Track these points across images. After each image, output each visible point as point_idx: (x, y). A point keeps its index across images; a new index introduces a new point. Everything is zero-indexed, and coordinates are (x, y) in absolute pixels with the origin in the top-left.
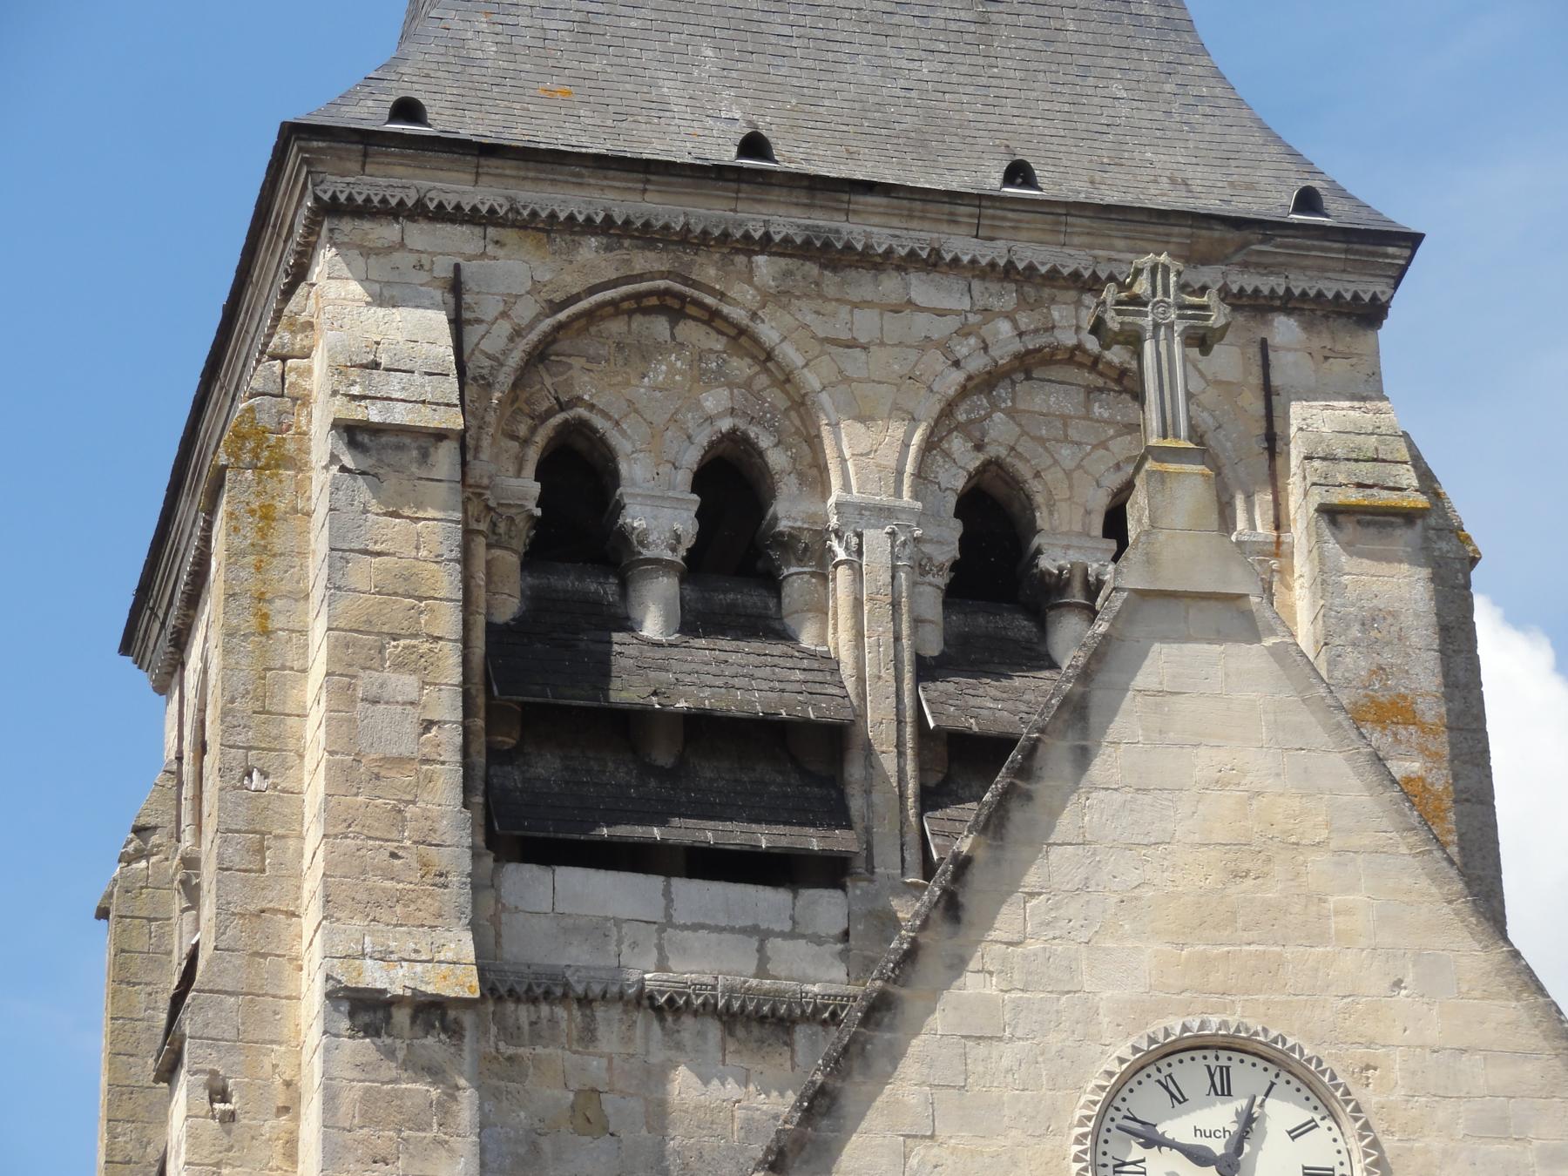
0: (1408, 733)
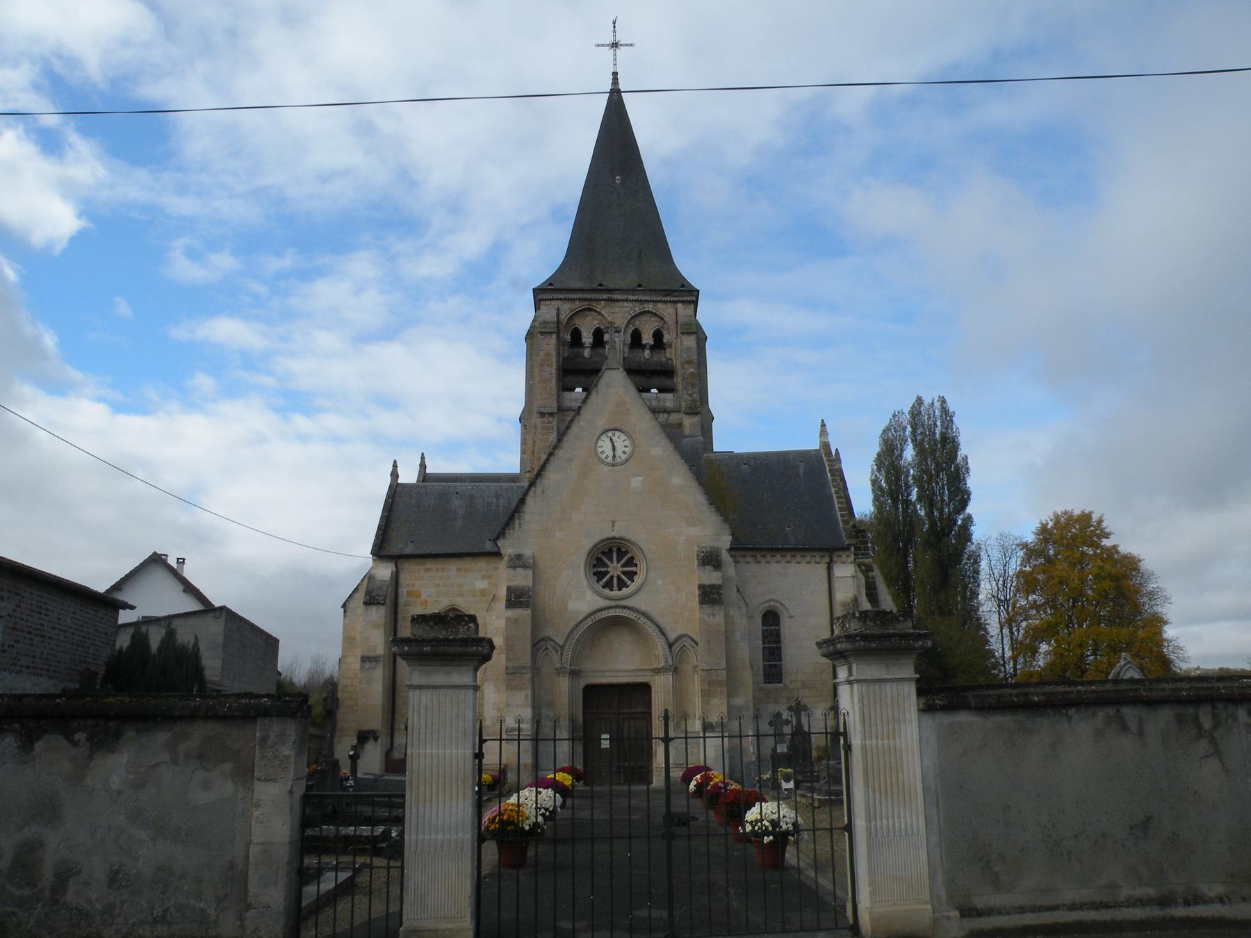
0: (692, 365)
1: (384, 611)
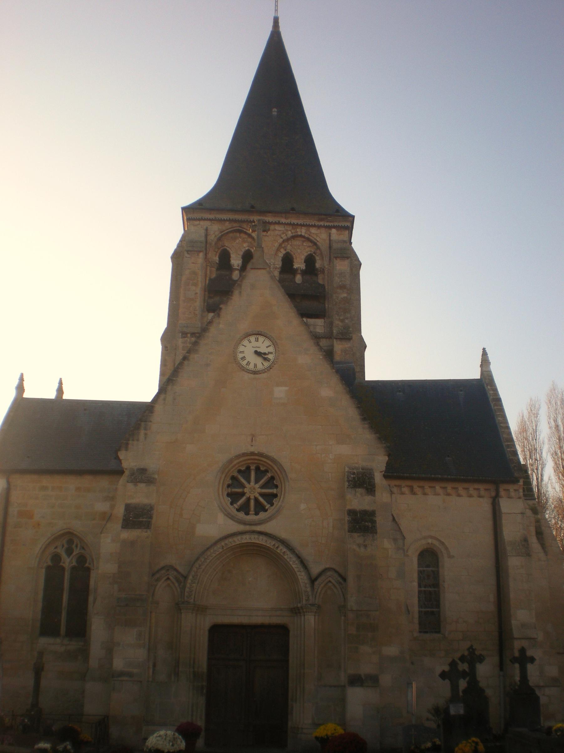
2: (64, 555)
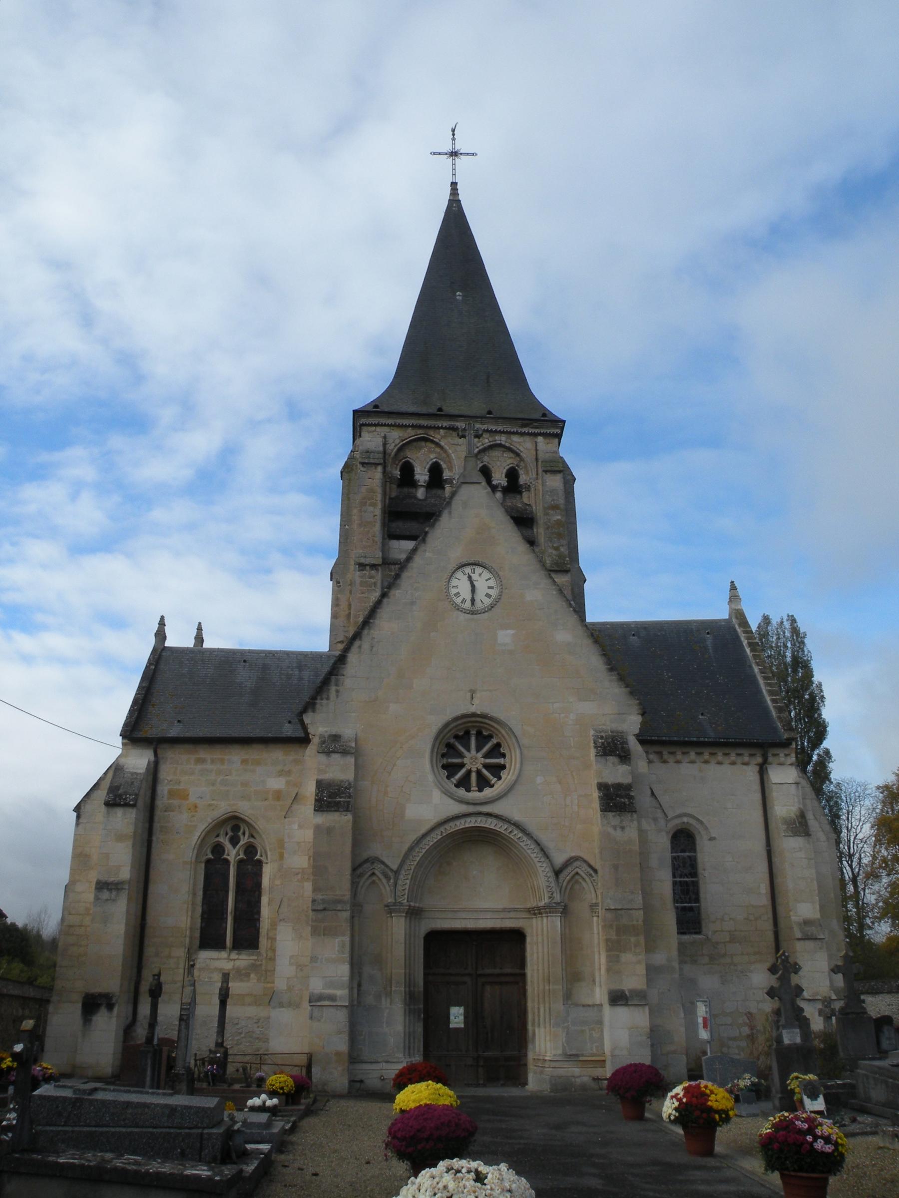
0: (558, 511)
1: (134, 816)
2: (228, 846)
